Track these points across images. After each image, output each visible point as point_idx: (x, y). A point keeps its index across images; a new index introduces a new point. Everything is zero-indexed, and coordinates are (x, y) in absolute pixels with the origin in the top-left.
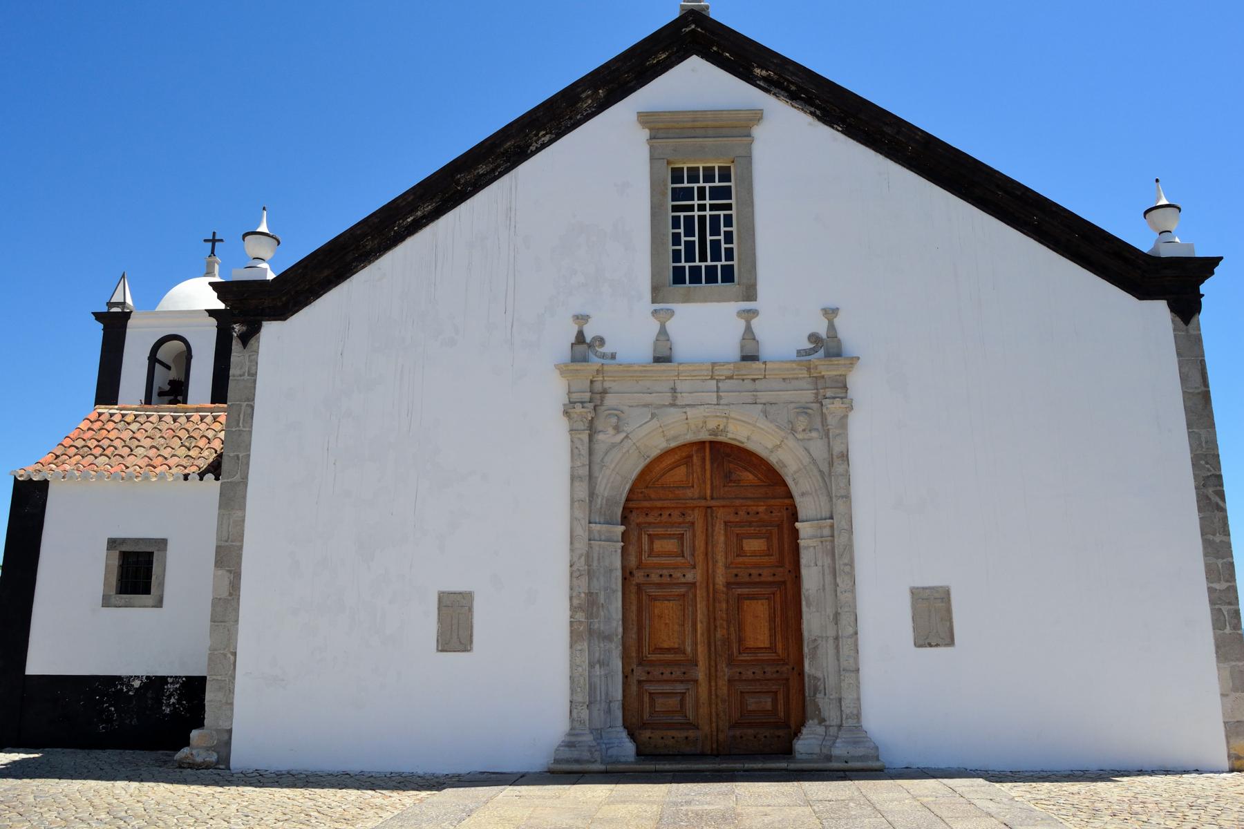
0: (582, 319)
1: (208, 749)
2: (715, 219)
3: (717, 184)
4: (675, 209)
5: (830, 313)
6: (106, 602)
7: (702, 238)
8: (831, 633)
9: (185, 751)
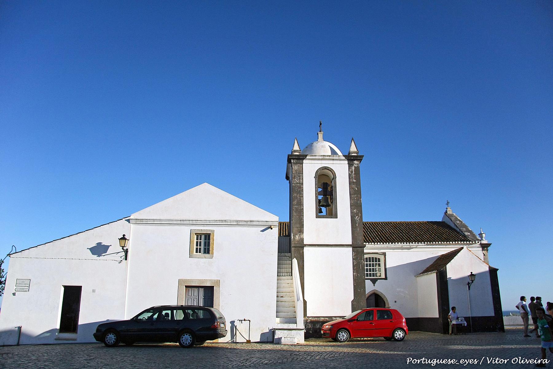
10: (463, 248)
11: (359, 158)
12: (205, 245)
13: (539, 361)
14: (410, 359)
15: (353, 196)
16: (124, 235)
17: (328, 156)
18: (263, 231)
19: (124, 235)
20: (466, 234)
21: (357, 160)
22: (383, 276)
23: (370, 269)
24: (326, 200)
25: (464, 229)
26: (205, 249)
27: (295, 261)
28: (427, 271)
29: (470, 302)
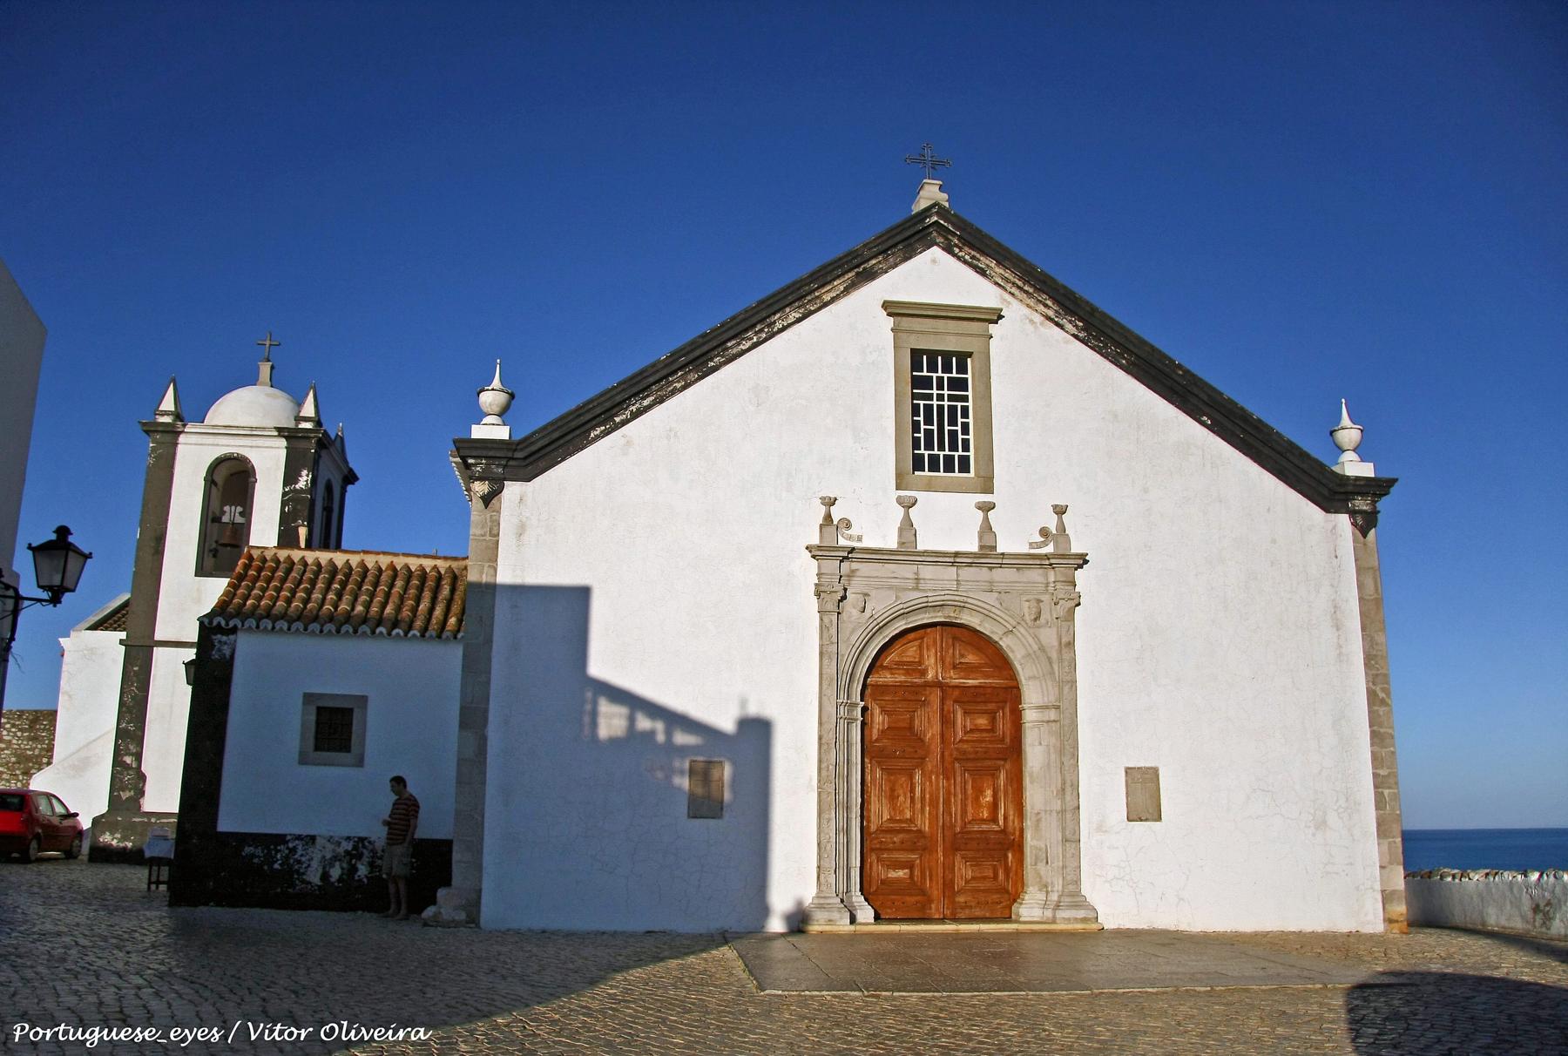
0: (830, 502)
1: (456, 908)
2: (953, 409)
3: (954, 375)
4: (914, 396)
5: (1060, 511)
6: (303, 760)
7: (940, 416)
8: (1057, 805)
9: (429, 912)
13: (401, 1034)
14: (23, 1029)
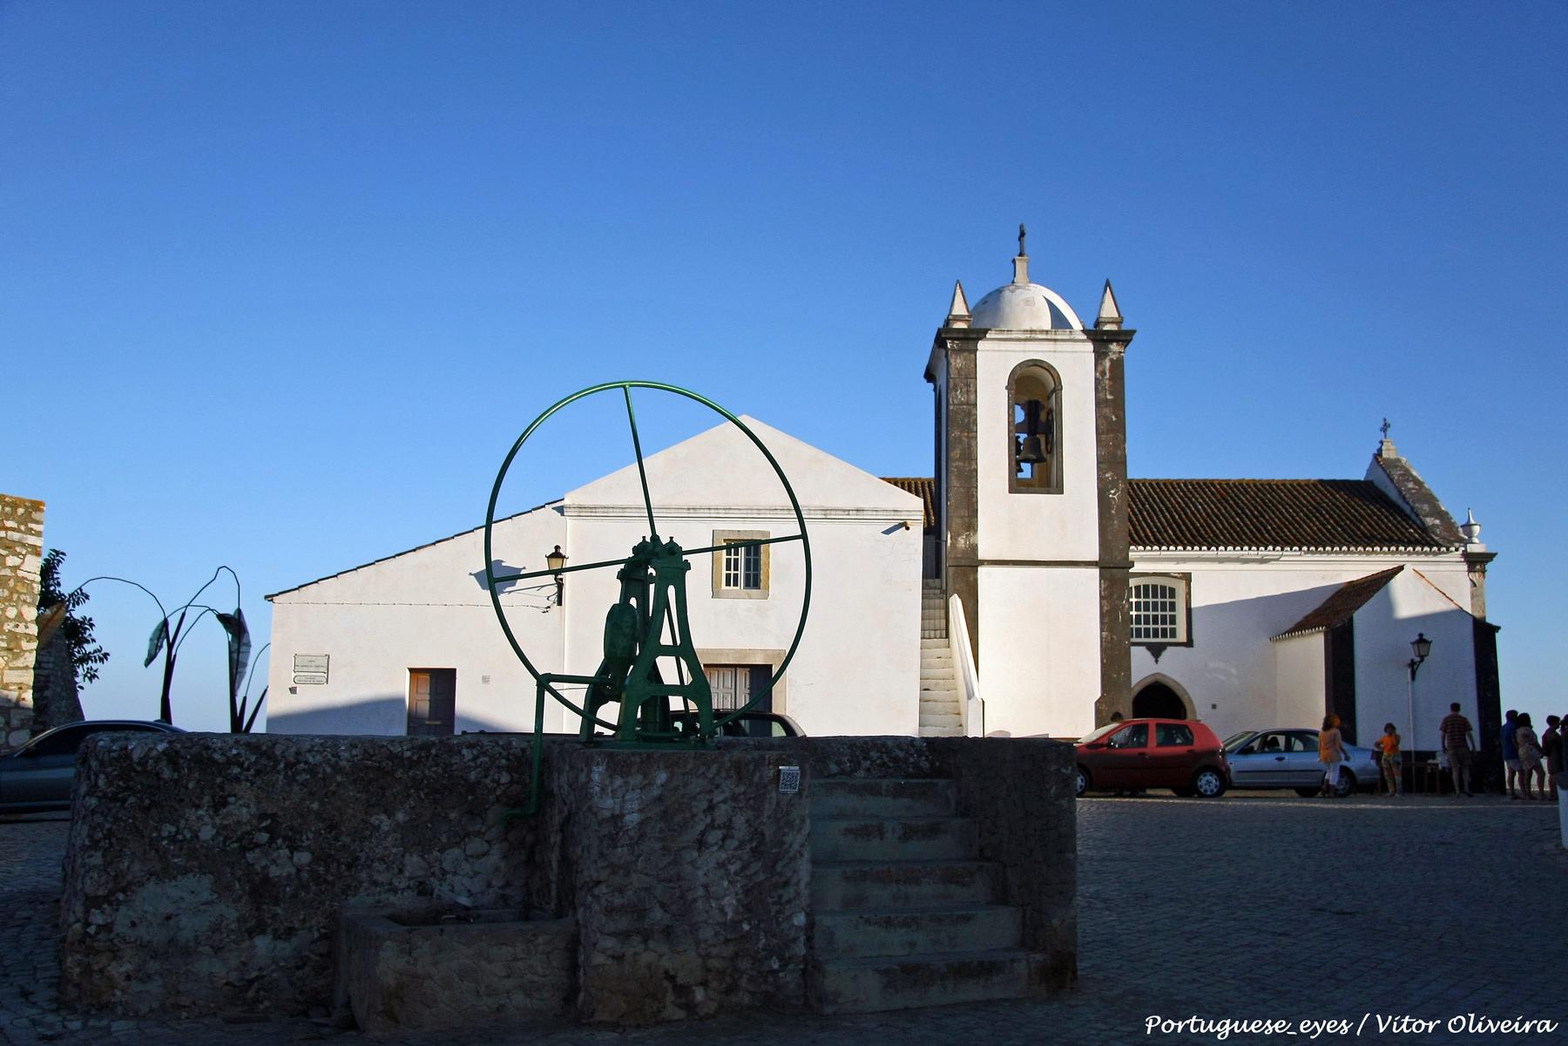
10: (1401, 568)
11: (1124, 337)
12: (747, 568)
15: (1104, 437)
16: (557, 548)
17: (1042, 332)
18: (887, 532)
19: (557, 548)
20: (1429, 521)
21: (1117, 341)
22: (1182, 636)
23: (1146, 617)
24: (1034, 445)
25: (1426, 507)
26: (747, 577)
27: (956, 603)
28: (1304, 626)
29: (1414, 711)
